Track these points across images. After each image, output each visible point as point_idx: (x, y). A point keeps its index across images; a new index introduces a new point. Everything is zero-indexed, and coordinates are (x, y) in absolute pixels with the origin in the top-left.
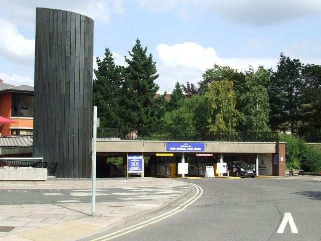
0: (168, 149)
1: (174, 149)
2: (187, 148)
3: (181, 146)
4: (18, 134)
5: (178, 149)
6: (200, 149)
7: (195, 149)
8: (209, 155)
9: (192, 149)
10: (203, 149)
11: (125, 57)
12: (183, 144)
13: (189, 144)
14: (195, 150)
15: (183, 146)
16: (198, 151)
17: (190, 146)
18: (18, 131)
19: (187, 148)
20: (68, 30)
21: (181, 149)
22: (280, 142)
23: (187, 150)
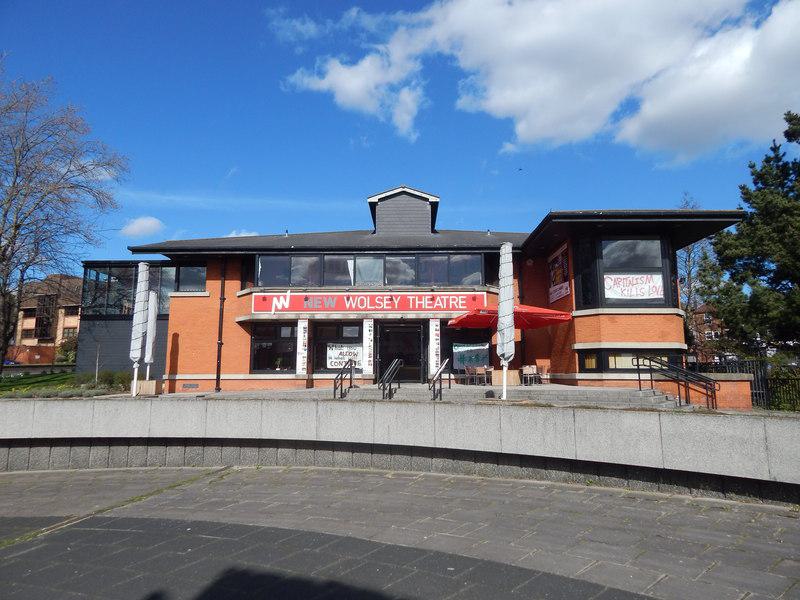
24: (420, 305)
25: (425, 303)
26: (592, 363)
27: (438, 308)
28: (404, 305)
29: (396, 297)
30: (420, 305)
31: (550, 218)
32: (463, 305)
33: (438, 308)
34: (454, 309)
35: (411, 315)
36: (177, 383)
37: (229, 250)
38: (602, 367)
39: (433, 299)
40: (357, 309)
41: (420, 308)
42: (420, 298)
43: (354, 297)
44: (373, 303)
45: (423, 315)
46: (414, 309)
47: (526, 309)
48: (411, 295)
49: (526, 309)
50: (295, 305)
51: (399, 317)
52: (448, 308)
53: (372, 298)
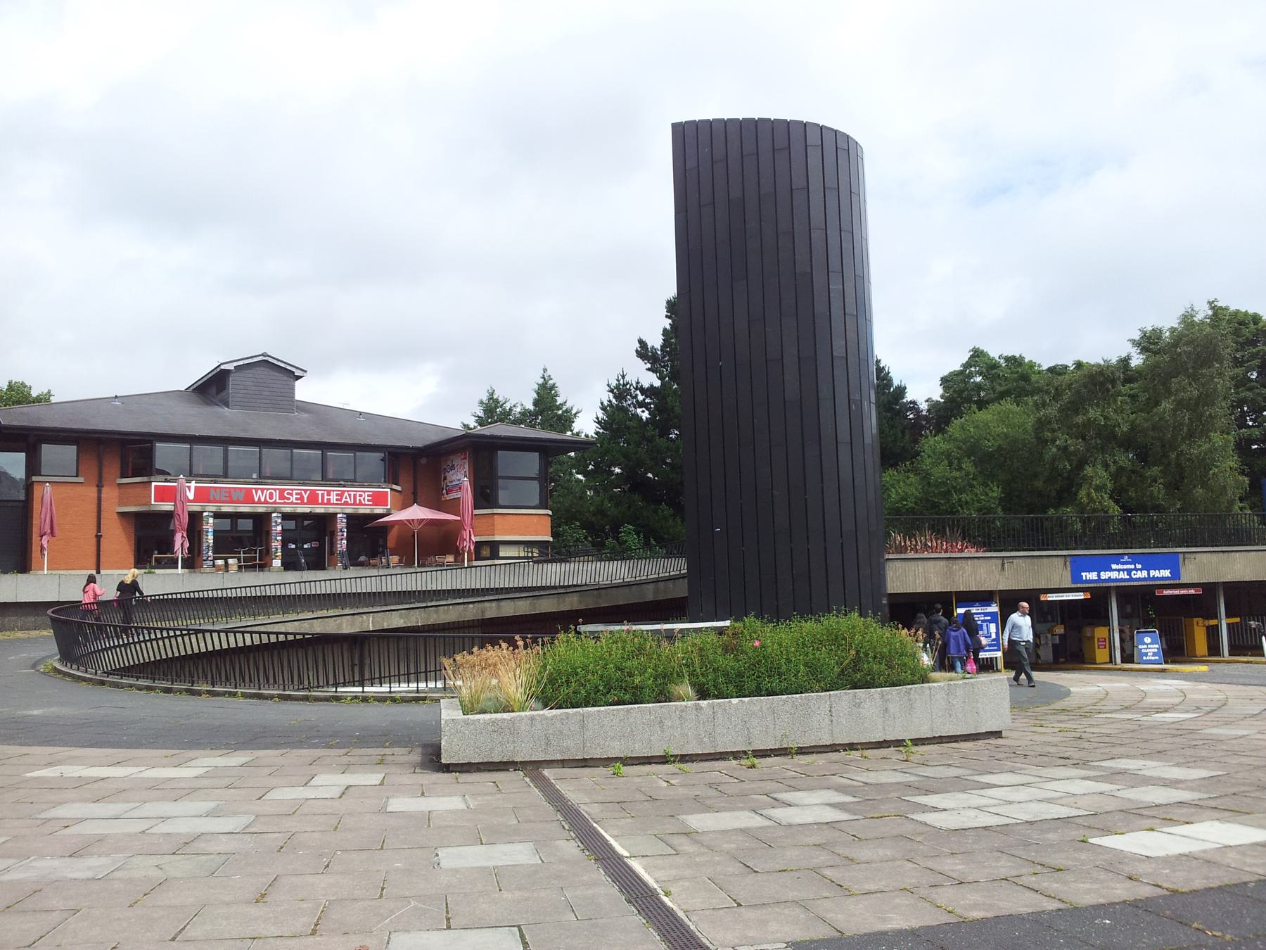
0: (1076, 577)
1: (1093, 576)
2: (1129, 571)
3: (1114, 566)
4: (494, 555)
5: (1105, 575)
6: (1167, 573)
7: (1153, 573)
8: (1192, 592)
9: (1145, 574)
10: (1176, 573)
11: (545, 370)
12: (1117, 559)
13: (1135, 559)
14: (1154, 579)
15: (1120, 567)
16: (1163, 578)
17: (1139, 566)
18: (494, 547)
19: (1129, 571)
20: (798, 182)
21: (1114, 575)
22: (887, 556)
23: (1131, 579)
24: (329, 500)
25: (333, 498)
26: (486, 552)
27: (346, 503)
28: (313, 499)
29: (305, 491)
30: (329, 500)
31: (669, 302)
32: (1154, 654)
33: (346, 503)
34: (361, 504)
35: (320, 510)
36: (536, 502)
37: (1132, 670)
38: (494, 555)
39: (341, 495)
40: (266, 502)
41: (329, 502)
42: (329, 493)
43: (262, 490)
44: (282, 497)
45: (331, 510)
46: (323, 503)
47: (341, 524)
48: (320, 490)
49: (341, 524)
50: (201, 495)
51: (308, 511)
52: (355, 504)
53: (282, 491)
